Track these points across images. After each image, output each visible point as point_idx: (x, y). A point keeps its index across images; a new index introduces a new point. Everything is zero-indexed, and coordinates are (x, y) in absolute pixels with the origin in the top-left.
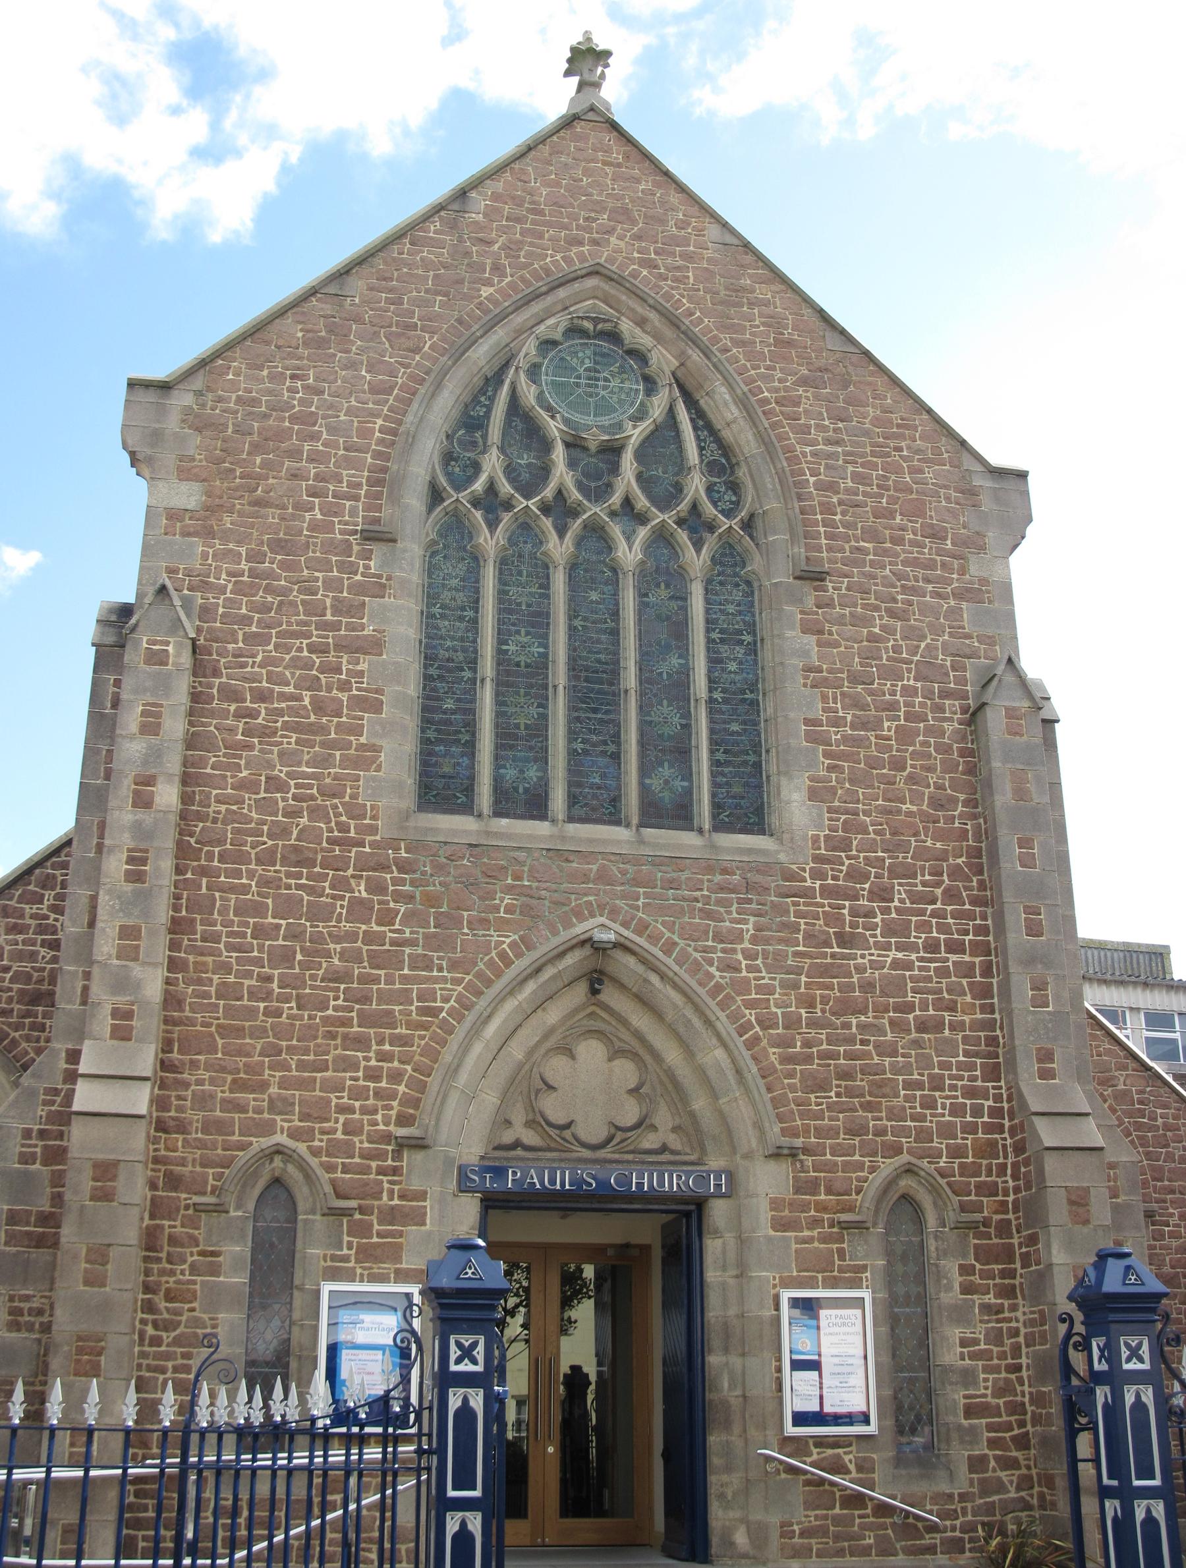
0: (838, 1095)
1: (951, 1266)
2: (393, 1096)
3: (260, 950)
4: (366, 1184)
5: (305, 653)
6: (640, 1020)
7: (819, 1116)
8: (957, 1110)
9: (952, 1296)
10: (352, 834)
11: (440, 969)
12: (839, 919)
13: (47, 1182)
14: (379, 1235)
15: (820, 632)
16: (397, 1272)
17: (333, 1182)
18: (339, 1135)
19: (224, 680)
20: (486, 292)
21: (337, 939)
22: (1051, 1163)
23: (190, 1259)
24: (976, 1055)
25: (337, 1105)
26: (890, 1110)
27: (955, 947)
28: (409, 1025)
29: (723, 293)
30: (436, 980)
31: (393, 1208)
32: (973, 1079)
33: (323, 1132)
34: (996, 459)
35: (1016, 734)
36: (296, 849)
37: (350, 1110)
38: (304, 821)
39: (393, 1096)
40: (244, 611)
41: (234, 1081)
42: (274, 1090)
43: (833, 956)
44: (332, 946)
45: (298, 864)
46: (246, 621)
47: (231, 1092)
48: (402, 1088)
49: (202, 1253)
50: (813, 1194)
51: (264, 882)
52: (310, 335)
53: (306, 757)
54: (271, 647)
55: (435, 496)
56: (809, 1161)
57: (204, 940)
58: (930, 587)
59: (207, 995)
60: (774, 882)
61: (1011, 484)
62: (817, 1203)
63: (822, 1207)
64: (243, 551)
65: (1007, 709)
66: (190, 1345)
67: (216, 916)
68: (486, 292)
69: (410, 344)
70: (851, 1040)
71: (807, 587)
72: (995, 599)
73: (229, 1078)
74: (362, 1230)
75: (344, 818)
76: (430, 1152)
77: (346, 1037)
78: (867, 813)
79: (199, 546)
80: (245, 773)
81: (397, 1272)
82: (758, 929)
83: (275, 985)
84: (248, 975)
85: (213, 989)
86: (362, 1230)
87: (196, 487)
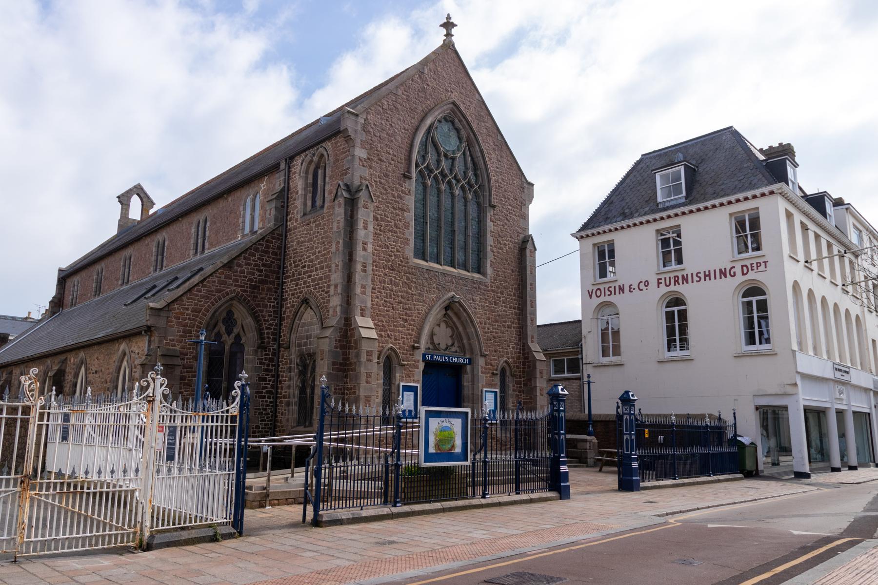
1: (511, 385)
6: (455, 319)
9: (511, 392)
22: (538, 363)
34: (529, 180)
55: (417, 166)
72: (525, 217)
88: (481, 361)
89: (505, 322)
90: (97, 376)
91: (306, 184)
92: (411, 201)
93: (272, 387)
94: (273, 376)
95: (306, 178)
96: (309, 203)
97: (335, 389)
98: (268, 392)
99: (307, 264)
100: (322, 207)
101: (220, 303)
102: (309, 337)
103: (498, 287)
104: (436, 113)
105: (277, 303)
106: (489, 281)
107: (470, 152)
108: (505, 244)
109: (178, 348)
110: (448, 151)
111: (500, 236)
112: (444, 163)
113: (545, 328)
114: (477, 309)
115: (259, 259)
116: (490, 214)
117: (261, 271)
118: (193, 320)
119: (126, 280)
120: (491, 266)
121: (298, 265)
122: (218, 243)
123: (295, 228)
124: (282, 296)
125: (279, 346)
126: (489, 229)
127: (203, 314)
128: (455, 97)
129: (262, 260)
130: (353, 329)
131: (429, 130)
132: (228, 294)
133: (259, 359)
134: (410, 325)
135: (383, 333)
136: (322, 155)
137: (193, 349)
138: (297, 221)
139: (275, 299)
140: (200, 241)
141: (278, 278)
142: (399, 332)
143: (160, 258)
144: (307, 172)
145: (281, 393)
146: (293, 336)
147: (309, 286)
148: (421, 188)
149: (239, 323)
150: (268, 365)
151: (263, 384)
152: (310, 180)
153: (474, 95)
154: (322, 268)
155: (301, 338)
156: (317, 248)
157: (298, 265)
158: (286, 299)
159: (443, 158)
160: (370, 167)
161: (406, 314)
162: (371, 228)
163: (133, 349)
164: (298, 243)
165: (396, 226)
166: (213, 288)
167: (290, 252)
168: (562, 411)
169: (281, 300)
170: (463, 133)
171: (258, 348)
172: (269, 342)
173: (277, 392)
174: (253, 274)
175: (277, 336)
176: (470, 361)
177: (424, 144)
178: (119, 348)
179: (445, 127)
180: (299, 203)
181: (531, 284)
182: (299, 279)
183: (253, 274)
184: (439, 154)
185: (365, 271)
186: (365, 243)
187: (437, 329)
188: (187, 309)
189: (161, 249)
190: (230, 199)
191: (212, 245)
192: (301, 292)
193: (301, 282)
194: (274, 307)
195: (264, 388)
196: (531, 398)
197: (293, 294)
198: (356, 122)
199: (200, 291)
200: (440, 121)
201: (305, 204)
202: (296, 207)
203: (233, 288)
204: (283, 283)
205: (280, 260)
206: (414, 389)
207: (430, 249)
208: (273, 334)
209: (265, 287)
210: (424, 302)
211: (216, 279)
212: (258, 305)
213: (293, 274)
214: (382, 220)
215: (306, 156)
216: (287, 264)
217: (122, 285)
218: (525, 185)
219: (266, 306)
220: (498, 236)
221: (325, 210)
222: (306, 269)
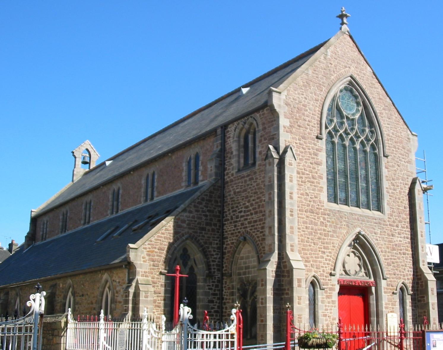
12: (392, 231)
14: (329, 293)
20: (332, 77)
21: (319, 230)
26: (400, 270)
29: (333, 66)
30: (335, 240)
38: (312, 203)
42: (311, 262)
45: (312, 213)
51: (307, 217)
55: (326, 128)
60: (382, 222)
71: (386, 158)
77: (322, 251)
82: (381, 232)
86: (326, 292)
87: (288, 120)
88: (384, 283)
89: (401, 250)
90: (84, 298)
91: (239, 146)
93: (218, 307)
94: (218, 299)
95: (239, 141)
96: (242, 161)
98: (215, 312)
99: (243, 209)
100: (254, 164)
102: (247, 268)
103: (394, 222)
104: (338, 85)
105: (220, 241)
109: (150, 278)
110: (349, 114)
111: (393, 180)
115: (205, 206)
117: (206, 216)
119: (87, 221)
120: (388, 204)
121: (235, 211)
122: (165, 192)
123: (232, 181)
124: (223, 235)
125: (223, 275)
129: (207, 207)
130: (285, 262)
131: (333, 100)
132: (183, 235)
134: (328, 256)
136: (251, 124)
138: (232, 175)
139: (218, 238)
140: (150, 190)
141: (219, 221)
142: (320, 262)
143: (115, 203)
144: (239, 137)
145: (226, 312)
146: (234, 267)
147: (246, 227)
148: (330, 146)
149: (192, 257)
151: (211, 305)
152: (242, 143)
154: (256, 213)
155: (241, 268)
156: (251, 197)
157: (235, 211)
158: (227, 238)
160: (291, 132)
161: (324, 248)
162: (295, 182)
163: (114, 278)
164: (235, 193)
167: (228, 199)
169: (222, 239)
171: (207, 276)
172: (214, 272)
173: (222, 312)
174: (201, 218)
175: (220, 267)
177: (330, 109)
178: (102, 278)
180: (234, 161)
182: (236, 222)
185: (292, 215)
186: (291, 193)
188: (155, 248)
189: (116, 196)
190: (174, 157)
191: (160, 194)
192: (239, 232)
193: (239, 224)
195: (213, 308)
196: (425, 312)
197: (232, 234)
201: (239, 162)
202: (232, 164)
204: (223, 225)
207: (341, 195)
210: (337, 237)
212: (206, 243)
213: (232, 217)
214: (303, 174)
215: (238, 124)
216: (226, 210)
217: (84, 224)
221: (257, 167)
222: (243, 214)
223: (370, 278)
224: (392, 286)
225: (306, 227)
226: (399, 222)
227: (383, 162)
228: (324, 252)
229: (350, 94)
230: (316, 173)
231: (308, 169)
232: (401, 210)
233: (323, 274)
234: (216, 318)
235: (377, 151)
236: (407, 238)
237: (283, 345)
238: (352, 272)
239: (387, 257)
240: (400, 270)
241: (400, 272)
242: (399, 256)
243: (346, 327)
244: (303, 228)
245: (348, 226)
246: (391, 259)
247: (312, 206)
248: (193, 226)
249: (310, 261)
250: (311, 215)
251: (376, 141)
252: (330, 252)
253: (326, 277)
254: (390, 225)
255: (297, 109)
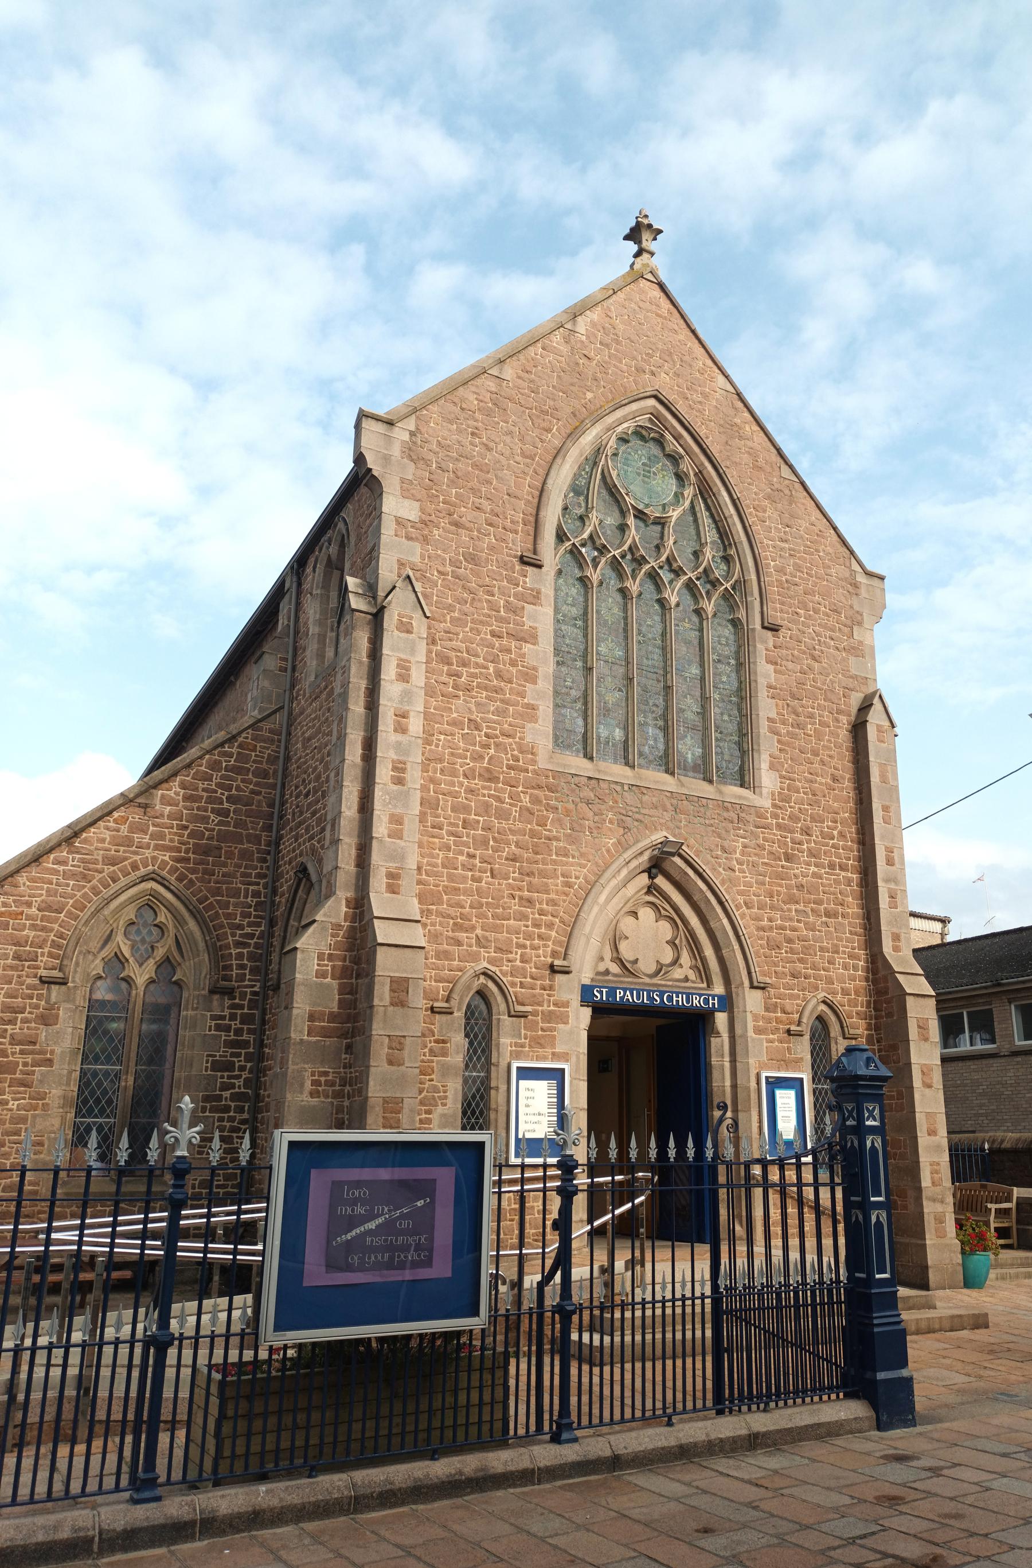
0: (786, 952)
2: (548, 939)
3: (468, 837)
4: (534, 996)
5: (489, 637)
7: (776, 965)
8: (845, 967)
10: (521, 763)
11: (573, 857)
12: (786, 844)
13: (336, 992)
14: (542, 1030)
15: (776, 664)
16: (553, 1054)
17: (516, 994)
18: (518, 963)
19: (439, 648)
20: (589, 395)
22: (910, 1001)
23: (429, 1045)
24: (856, 934)
25: (517, 943)
27: (843, 868)
28: (557, 892)
31: (550, 1012)
32: (853, 948)
33: (509, 961)
35: (882, 741)
36: (488, 770)
37: (524, 947)
38: (492, 751)
39: (548, 939)
40: (450, 601)
41: (455, 924)
42: (479, 931)
43: (783, 867)
44: (511, 837)
45: (490, 780)
46: (450, 608)
47: (453, 931)
48: (553, 934)
49: (437, 1041)
50: (774, 1012)
51: (471, 791)
52: (481, 404)
53: (492, 708)
54: (467, 629)
55: (561, 537)
56: (772, 991)
57: (433, 827)
58: (832, 643)
59: (435, 865)
60: (752, 818)
61: (876, 582)
62: (777, 1018)
63: (778, 1021)
64: (447, 557)
65: (878, 725)
66: (430, 1105)
67: (440, 811)
68: (589, 395)
69: (545, 425)
70: (791, 919)
71: (769, 633)
73: (452, 921)
74: (532, 1027)
75: (516, 752)
76: (571, 975)
77: (521, 898)
78: (799, 781)
79: (417, 547)
80: (455, 715)
81: (553, 1054)
82: (745, 846)
83: (477, 861)
84: (461, 853)
85: (440, 861)
86: (532, 1027)
87: (417, 504)
88: (752, 1002)
92: (542, 618)
97: (315, 1083)
101: (114, 887)
103: (793, 818)
105: (265, 887)
106: (767, 803)
107: (708, 508)
108: (811, 716)
112: (634, 533)
113: (1006, 937)
114: (736, 873)
116: (763, 643)
117: (226, 813)
118: (43, 929)
120: (772, 767)
126: (762, 682)
127: (69, 914)
128: (664, 382)
129: (229, 788)
133: (213, 1018)
135: (462, 935)
137: (39, 997)
139: (260, 876)
141: (268, 828)
150: (238, 1032)
153: (712, 379)
159: (631, 521)
160: (426, 540)
162: (418, 677)
165: (499, 675)
166: (99, 855)
168: (872, 1130)
170: (686, 466)
171: (212, 992)
172: (241, 978)
174: (205, 820)
176: (727, 1003)
179: (641, 453)
181: (886, 809)
183: (205, 820)
184: (623, 513)
185: (399, 781)
187: (627, 924)
188: (29, 905)
194: (256, 894)
195: (225, 1087)
198: (388, 439)
199: (64, 863)
200: (623, 440)
203: (148, 853)
205: (273, 786)
206: (796, 1084)
208: (252, 957)
209: (237, 848)
211: (107, 835)
218: (861, 578)
219: (236, 894)
220: (790, 697)
222: (310, 799)
223: (710, 984)
224: (784, 1012)
225: (464, 821)
226: (813, 819)
227: (760, 646)
228: (530, 902)
229: (655, 450)
230: (513, 663)
231: (482, 651)
232: (821, 784)
233: (523, 968)
234: (238, 1117)
235: (742, 614)
236: (841, 869)
237: (187, 1217)
238: (647, 966)
239: (765, 923)
240: (813, 963)
241: (814, 967)
242: (811, 919)
243: (124, 1143)
244: (451, 824)
245: (621, 824)
246: (783, 928)
247: (491, 758)
248: (171, 841)
249: (473, 928)
250: (484, 788)
251: (741, 585)
252: (553, 902)
253: (532, 978)
254: (779, 826)
255: (451, 475)
